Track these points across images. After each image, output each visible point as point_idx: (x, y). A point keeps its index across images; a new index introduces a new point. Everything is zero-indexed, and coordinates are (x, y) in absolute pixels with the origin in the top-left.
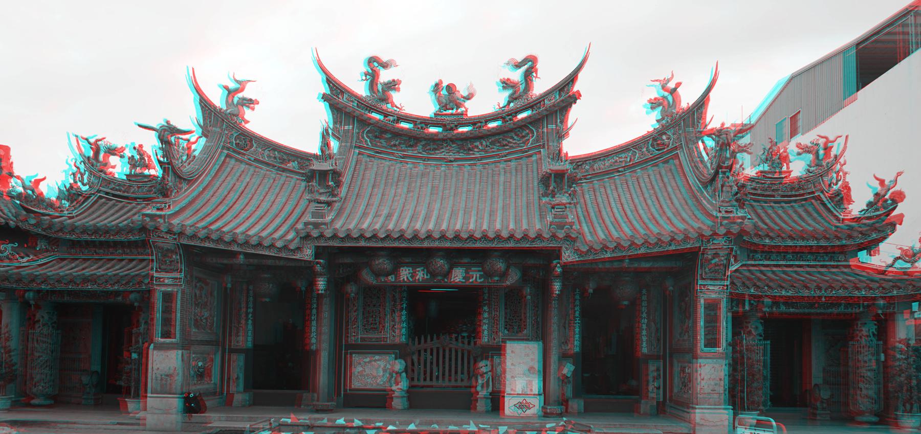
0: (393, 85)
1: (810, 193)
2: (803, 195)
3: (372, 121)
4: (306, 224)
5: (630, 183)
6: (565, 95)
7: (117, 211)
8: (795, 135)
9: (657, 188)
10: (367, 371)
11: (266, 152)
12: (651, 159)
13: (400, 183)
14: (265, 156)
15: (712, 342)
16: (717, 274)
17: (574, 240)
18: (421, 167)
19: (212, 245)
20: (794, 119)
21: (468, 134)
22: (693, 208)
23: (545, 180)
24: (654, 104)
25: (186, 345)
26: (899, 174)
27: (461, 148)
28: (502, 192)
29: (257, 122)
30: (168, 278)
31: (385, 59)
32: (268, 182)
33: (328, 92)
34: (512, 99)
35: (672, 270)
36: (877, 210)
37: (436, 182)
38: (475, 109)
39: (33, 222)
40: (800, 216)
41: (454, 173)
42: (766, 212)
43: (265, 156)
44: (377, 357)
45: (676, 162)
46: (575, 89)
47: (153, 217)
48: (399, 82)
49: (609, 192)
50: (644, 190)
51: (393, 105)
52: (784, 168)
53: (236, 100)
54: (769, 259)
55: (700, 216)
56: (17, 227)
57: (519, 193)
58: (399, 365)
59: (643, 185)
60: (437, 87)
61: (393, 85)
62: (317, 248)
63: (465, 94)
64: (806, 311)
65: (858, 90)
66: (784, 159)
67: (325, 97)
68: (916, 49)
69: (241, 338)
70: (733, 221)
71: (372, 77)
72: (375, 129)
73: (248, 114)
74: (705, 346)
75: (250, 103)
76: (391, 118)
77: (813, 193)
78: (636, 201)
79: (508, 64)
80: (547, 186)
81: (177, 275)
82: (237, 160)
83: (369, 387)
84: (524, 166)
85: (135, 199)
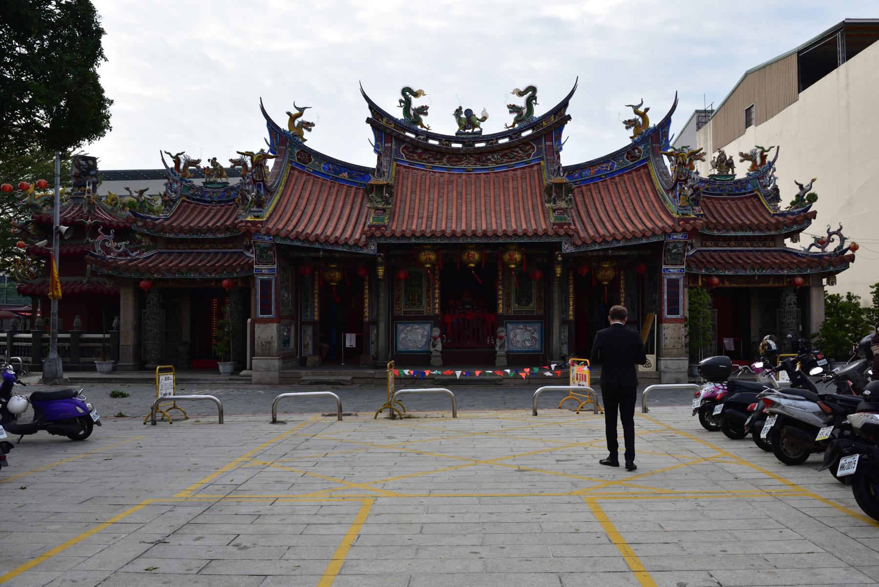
0: (423, 110)
1: (750, 193)
2: (744, 194)
3: (408, 140)
4: (370, 227)
5: (610, 188)
6: (559, 116)
7: (199, 213)
8: (750, 125)
9: (631, 192)
10: (409, 337)
11: (322, 165)
12: (626, 168)
13: (432, 190)
14: (322, 167)
15: (265, 309)
16: (676, 260)
17: (571, 236)
18: (447, 176)
19: (299, 244)
20: (748, 111)
21: (483, 150)
22: (659, 210)
23: (548, 190)
24: (629, 124)
25: (278, 320)
26: (813, 180)
27: (478, 160)
28: (511, 197)
29: (313, 141)
30: (264, 268)
31: (415, 90)
32: (326, 189)
33: (370, 116)
34: (517, 120)
35: (640, 260)
36: (797, 207)
37: (459, 189)
38: (487, 129)
39: (140, 224)
40: (742, 211)
41: (473, 181)
42: (715, 208)
43: (322, 167)
44: (416, 326)
45: (646, 170)
46: (567, 113)
47: (254, 223)
48: (427, 108)
49: (595, 195)
50: (622, 194)
51: (422, 126)
52: (730, 173)
53: (296, 123)
54: (717, 246)
55: (663, 216)
56: (125, 226)
57: (525, 198)
58: (437, 332)
59: (620, 190)
60: (458, 112)
61: (423, 110)
62: (378, 244)
63: (480, 117)
64: (744, 285)
65: (799, 92)
66: (730, 164)
67: (368, 121)
68: (850, 55)
69: (309, 314)
70: (687, 221)
71: (406, 104)
72: (409, 146)
73: (306, 134)
74: (262, 281)
75: (308, 126)
76: (422, 137)
77: (753, 192)
78: (616, 203)
79: (513, 93)
80: (550, 195)
81: (270, 267)
82: (299, 171)
83: (411, 349)
84: (528, 175)
85: (210, 202)
